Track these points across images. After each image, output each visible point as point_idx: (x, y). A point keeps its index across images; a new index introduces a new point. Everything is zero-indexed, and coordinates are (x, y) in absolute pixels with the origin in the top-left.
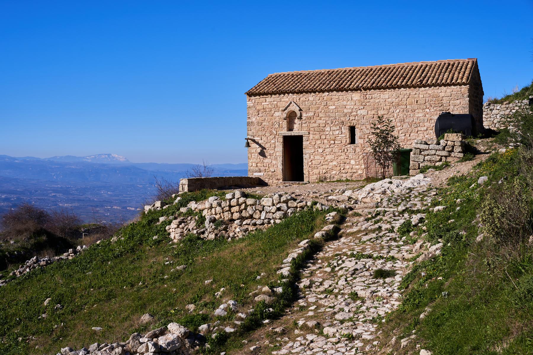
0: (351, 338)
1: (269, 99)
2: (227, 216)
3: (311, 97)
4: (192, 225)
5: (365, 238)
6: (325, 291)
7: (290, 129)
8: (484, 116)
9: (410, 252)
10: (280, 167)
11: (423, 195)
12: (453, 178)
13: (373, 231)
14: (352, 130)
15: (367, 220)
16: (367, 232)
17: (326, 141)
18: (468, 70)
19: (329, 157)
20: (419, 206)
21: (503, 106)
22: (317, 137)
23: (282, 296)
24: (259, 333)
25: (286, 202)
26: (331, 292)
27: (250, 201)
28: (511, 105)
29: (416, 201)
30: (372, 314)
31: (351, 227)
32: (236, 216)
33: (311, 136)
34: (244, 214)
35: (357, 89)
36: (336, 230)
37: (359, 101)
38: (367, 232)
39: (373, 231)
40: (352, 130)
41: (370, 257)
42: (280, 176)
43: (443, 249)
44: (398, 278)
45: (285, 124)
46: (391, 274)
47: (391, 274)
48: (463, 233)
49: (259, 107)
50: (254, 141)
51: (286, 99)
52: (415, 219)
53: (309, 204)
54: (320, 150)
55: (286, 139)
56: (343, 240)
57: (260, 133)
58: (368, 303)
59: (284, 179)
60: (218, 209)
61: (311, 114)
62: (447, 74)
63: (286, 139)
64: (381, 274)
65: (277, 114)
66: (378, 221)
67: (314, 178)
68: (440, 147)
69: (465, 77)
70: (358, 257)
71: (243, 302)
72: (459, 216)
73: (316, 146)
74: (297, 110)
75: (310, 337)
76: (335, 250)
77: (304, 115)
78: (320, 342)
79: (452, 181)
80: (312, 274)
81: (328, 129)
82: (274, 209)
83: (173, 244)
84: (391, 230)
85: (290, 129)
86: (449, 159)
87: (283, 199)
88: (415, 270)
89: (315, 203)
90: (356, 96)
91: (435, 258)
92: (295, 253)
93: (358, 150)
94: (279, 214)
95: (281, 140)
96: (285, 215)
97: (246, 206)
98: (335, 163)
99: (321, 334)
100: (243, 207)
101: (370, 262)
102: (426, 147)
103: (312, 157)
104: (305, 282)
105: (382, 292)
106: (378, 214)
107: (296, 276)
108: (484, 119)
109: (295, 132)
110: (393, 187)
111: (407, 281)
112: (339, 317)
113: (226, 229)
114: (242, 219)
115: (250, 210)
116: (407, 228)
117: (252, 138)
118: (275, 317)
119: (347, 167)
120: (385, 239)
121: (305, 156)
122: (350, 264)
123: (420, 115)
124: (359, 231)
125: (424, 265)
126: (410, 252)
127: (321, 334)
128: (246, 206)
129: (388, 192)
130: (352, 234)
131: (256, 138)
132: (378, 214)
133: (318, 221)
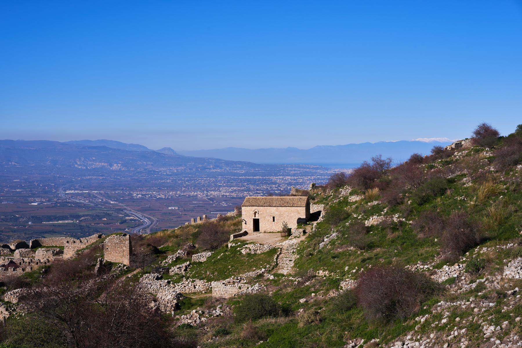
0: (288, 269)
1: (249, 207)
2: (256, 249)
3: (261, 208)
4: (248, 250)
5: (286, 254)
6: (282, 263)
7: (255, 217)
8: (311, 208)
9: (294, 257)
10: (252, 228)
11: (296, 245)
12: (301, 241)
13: (288, 253)
14: (274, 218)
15: (286, 250)
16: (287, 253)
17: (266, 221)
18: (305, 201)
19: (267, 225)
20: (295, 248)
21: (317, 205)
22: (263, 219)
23: (276, 264)
24: (274, 269)
25: (269, 246)
26: (283, 263)
27: (262, 246)
28: (319, 205)
29: (294, 246)
30: (290, 266)
31: (283, 252)
32: (258, 249)
33: (262, 219)
34: (260, 248)
35: (275, 206)
36: (281, 252)
37: (276, 210)
38: (287, 253)
39: (288, 253)
40: (274, 218)
41: (288, 258)
42: (252, 230)
43: (300, 256)
44: (293, 261)
45: (254, 215)
46: (292, 260)
47: (292, 260)
48: (302, 254)
49: (246, 210)
50: (244, 220)
51: (254, 208)
52: (295, 250)
53: (274, 247)
54: (264, 223)
55: (254, 219)
56: (282, 254)
57: (246, 218)
58: (289, 265)
59: (253, 231)
60: (254, 247)
61: (262, 213)
62: (300, 202)
63: (254, 219)
64: (290, 260)
65: (251, 212)
66: (288, 251)
67: (263, 231)
68: (298, 232)
69: (304, 205)
70: (286, 258)
71: (271, 265)
72: (302, 250)
73: (263, 222)
74: (257, 211)
75: (282, 270)
76: (282, 256)
77: (259, 213)
78: (284, 270)
79: (301, 241)
80: (279, 261)
81: (267, 217)
82: (267, 248)
83: (244, 255)
84: (291, 253)
85: (255, 217)
86: (300, 235)
87: (269, 246)
88: (296, 260)
89: (275, 247)
90: (275, 208)
91: (298, 258)
92: (275, 257)
93: (275, 223)
94: (268, 249)
95: (253, 220)
96: (269, 249)
97: (261, 247)
98: (269, 227)
99: (283, 269)
100: (260, 247)
101: (288, 259)
102: (295, 232)
103: (262, 225)
104: (278, 262)
105: (291, 263)
106: (288, 249)
107: (277, 261)
108: (311, 209)
109: (257, 218)
110: (290, 242)
111: (294, 262)
112: (285, 267)
113: (256, 252)
114: (260, 249)
115: (262, 248)
116: (293, 252)
117: (243, 219)
118: (276, 267)
119: (272, 228)
120: (290, 254)
121: (260, 225)
122: (285, 259)
123: (293, 215)
124: (285, 253)
125: (297, 259)
126: (294, 257)
127: (283, 269)
128: (261, 247)
129: (289, 244)
130: (284, 253)
131: (245, 219)
132: (288, 249)
133: (277, 250)
